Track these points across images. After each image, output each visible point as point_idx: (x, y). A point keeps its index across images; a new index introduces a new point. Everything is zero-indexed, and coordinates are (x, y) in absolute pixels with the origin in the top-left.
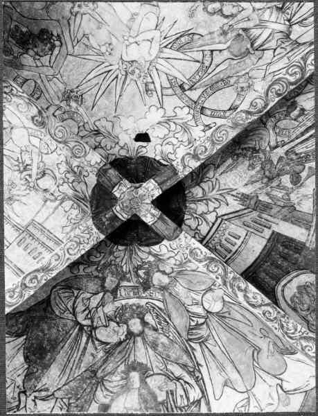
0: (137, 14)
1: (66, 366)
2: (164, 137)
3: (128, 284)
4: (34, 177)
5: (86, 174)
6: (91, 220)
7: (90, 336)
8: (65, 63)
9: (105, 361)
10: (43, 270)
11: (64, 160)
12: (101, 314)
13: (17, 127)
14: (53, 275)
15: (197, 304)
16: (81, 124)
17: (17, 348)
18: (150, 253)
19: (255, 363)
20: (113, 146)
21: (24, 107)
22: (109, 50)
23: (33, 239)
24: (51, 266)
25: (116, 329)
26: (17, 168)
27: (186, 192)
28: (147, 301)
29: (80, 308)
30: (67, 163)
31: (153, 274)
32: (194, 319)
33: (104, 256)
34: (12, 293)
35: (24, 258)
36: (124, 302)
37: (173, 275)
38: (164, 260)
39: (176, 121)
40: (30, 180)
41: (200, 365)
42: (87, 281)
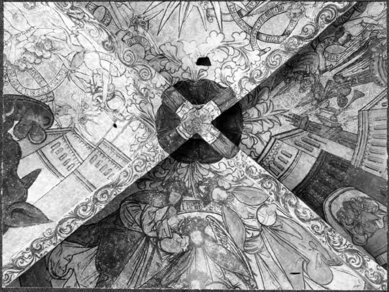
1: (133, 274)
3: (190, 199)
4: (105, 98)
5: (152, 96)
6: (157, 138)
7: (155, 247)
9: (169, 270)
13: (90, 52)
14: (122, 191)
15: (252, 218)
17: (89, 258)
18: (210, 170)
20: (177, 69)
21: (95, 33)
23: (104, 156)
24: (121, 182)
25: (179, 240)
26: (89, 90)
27: (243, 113)
28: (207, 214)
29: (147, 220)
30: (135, 85)
31: (213, 189)
32: (249, 231)
36: (186, 215)
37: (230, 190)
38: (222, 176)
40: (101, 101)
41: (255, 274)
42: (153, 196)
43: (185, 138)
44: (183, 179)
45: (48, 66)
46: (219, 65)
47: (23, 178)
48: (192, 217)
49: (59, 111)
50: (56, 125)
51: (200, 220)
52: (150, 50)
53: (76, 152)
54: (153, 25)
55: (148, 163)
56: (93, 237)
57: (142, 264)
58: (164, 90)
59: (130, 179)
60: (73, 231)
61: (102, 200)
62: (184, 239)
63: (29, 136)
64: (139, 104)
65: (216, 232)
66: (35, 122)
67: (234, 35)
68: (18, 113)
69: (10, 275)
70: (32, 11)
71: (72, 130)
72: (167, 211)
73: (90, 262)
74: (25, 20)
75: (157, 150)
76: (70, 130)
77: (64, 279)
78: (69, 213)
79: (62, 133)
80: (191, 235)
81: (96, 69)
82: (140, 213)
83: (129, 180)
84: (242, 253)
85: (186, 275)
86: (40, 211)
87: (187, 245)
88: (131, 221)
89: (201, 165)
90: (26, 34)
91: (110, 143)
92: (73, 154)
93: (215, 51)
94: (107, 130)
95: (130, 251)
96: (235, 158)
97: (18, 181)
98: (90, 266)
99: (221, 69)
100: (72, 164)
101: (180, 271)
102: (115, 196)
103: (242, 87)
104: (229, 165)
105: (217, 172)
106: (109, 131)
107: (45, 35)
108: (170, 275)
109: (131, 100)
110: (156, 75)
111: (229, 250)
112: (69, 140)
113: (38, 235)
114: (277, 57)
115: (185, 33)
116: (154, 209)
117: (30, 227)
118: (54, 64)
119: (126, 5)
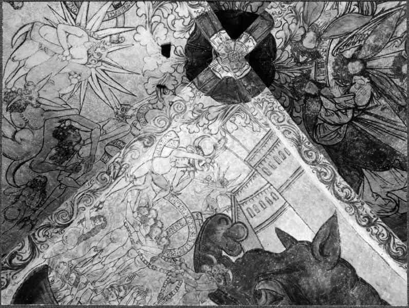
0: (41, 45)
1: (394, 134)
2: (166, 28)
3: (313, 72)
4: (201, 157)
5: (200, 106)
6: (247, 104)
7: (364, 111)
8: (88, 117)
9: (390, 97)
10: (299, 145)
11: (186, 125)
12: (342, 100)
13: (152, 167)
14: (305, 136)
16: (150, 106)
17: (375, 177)
18: (283, 49)
20: (174, 78)
21: (135, 154)
22: (76, 76)
23: (264, 160)
24: (295, 137)
25: (358, 86)
26: (191, 174)
27: (224, 9)
28: (330, 55)
29: (335, 119)
30: (189, 123)
31: (304, 47)
32: (351, 10)
33: (284, 93)
34: (322, 174)
35: (284, 168)
36: (331, 78)
37: (306, 28)
38: (290, 36)
39: (151, 15)
40: (204, 162)
42: (309, 110)
43: (249, 70)
44: (292, 78)
45: (164, 214)
46: (170, 33)
47: (285, 247)
48: (333, 71)
49: (212, 208)
50: (227, 211)
51: (336, 63)
52: (152, 104)
53: (257, 191)
54: (126, 101)
55: (275, 109)
56: (352, 173)
57: (382, 125)
58: (196, 89)
59: (293, 128)
60: (348, 186)
61: (315, 157)
62: (356, 81)
63: (238, 240)
64: (209, 120)
66: (224, 233)
67: (140, 14)
68: (214, 251)
69: (397, 246)
70: (108, 220)
71: (234, 195)
72: (325, 97)
73: (380, 177)
74: (117, 230)
75: (261, 99)
76: (234, 197)
77: (399, 201)
78: (329, 189)
79: (236, 205)
80: (352, 72)
81: (171, 163)
82: (327, 125)
83: (294, 129)
84: (375, 18)
85: (395, 80)
86: (323, 225)
87: (363, 78)
88: (335, 135)
89: (277, 58)
90: (132, 232)
91: (250, 154)
92: (260, 195)
93: (156, 37)
94: (236, 157)
95: (368, 138)
96: (273, 17)
97: (289, 251)
98: (384, 176)
99: (175, 31)
100: (271, 195)
101: (391, 86)
102: (311, 144)
103: (197, 5)
104: (279, 27)
105: (285, 41)
106: (237, 155)
107: (133, 212)
108: (395, 96)
109: (204, 129)
110: (180, 95)
111: (371, 33)
112: (244, 198)
113: (352, 222)
115: (135, 67)
116: (323, 110)
117: (340, 236)
118: (164, 208)
119: (104, 125)
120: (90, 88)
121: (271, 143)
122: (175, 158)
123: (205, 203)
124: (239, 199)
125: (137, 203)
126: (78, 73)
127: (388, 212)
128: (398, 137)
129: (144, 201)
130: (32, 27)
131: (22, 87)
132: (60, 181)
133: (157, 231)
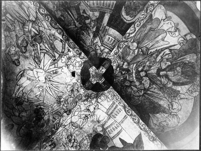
0: (27, 78)
1: (159, 98)
3: (128, 77)
4: (90, 113)
9: (157, 84)
12: (139, 86)
13: (71, 120)
14: (127, 105)
15: (134, 52)
16: (69, 96)
18: (116, 70)
19: (156, 30)
22: (41, 87)
23: (113, 112)
24: (123, 105)
26: (87, 120)
28: (133, 70)
29: (137, 94)
30: (84, 101)
31: (123, 68)
34: (134, 119)
36: (134, 78)
37: (124, 61)
39: (67, 62)
40: (91, 115)
42: (127, 92)
48: (135, 76)
49: (95, 131)
51: (136, 73)
57: (155, 95)
65: (141, 66)
67: (63, 62)
72: (133, 86)
79: (104, 130)
87: (146, 78)
96: (111, 60)
101: (157, 80)
114: (71, 44)
120: (47, 92)
121: (115, 106)
122: (80, 115)
123: (92, 130)
124: (105, 127)
125: (67, 135)
126: (42, 86)
127: (160, 132)
128: (161, 99)
129: (69, 133)
130: (24, 72)
131: (21, 95)
132: (37, 132)
133: (75, 144)
